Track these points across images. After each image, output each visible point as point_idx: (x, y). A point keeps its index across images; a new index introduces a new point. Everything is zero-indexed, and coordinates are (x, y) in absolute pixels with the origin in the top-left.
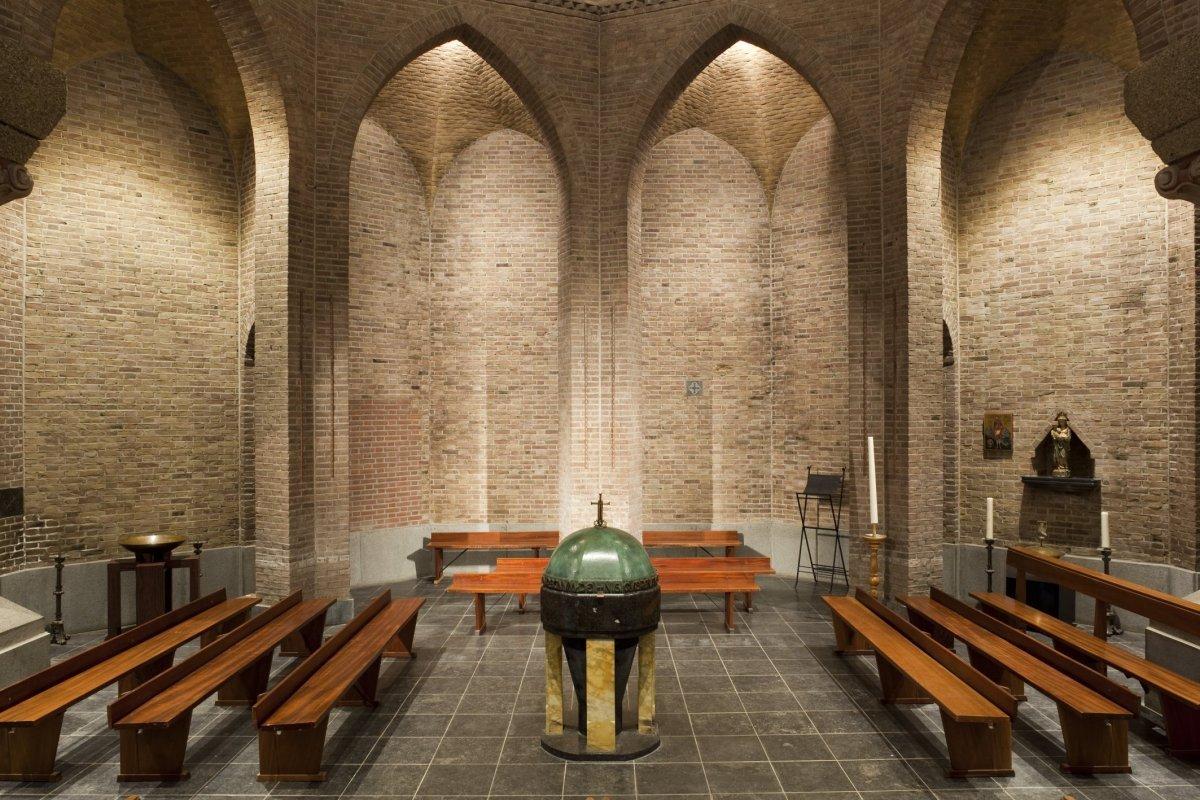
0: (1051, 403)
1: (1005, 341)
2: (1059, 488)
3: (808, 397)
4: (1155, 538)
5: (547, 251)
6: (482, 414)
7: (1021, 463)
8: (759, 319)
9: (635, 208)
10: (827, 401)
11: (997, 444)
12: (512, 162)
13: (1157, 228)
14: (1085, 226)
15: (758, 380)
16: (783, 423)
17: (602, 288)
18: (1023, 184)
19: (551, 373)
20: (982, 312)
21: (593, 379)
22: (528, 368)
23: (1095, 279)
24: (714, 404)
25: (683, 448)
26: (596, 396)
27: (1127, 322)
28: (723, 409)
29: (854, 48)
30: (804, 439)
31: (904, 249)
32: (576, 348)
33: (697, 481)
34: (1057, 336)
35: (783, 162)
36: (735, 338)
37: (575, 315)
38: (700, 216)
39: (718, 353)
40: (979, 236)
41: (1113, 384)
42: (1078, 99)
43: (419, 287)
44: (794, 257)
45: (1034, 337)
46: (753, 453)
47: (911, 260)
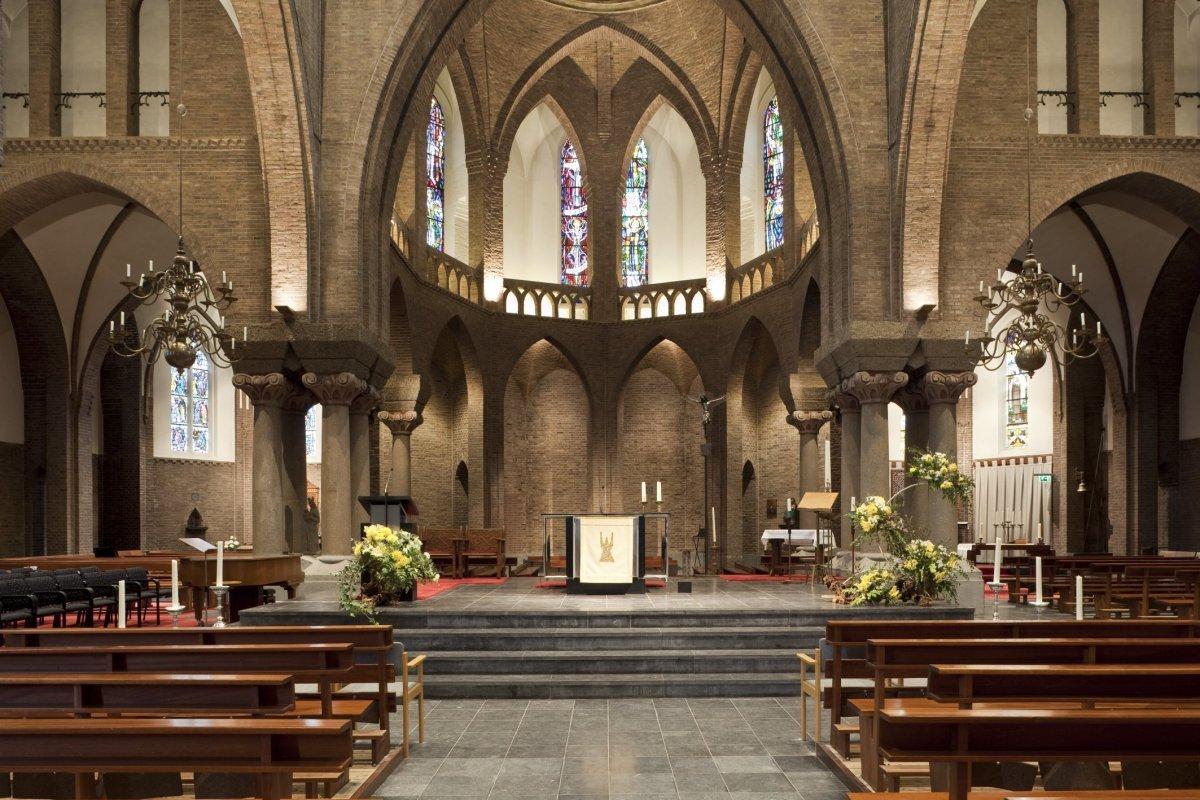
6: (551, 502)
9: (621, 411)
16: (690, 506)
32: (596, 472)
43: (521, 443)
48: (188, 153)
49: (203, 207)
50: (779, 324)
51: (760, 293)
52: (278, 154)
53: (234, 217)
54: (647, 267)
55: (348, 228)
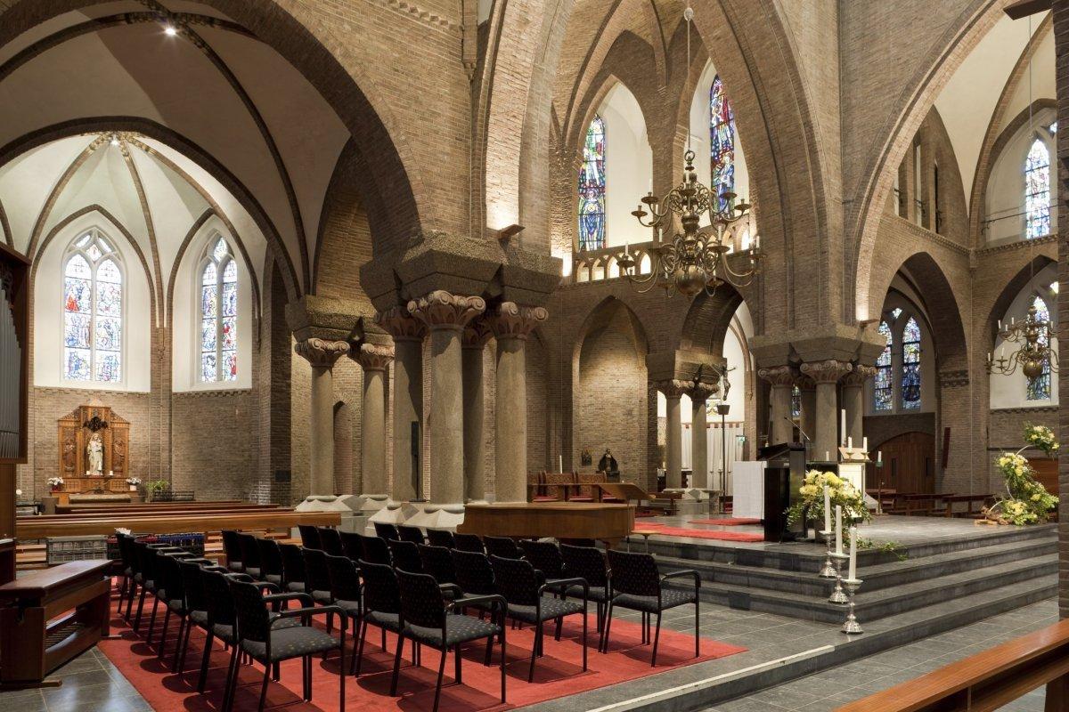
23: (618, 405)
31: (571, 392)
48: (387, 12)
49: (403, 83)
52: (511, 58)
53: (435, 107)
55: (540, 156)
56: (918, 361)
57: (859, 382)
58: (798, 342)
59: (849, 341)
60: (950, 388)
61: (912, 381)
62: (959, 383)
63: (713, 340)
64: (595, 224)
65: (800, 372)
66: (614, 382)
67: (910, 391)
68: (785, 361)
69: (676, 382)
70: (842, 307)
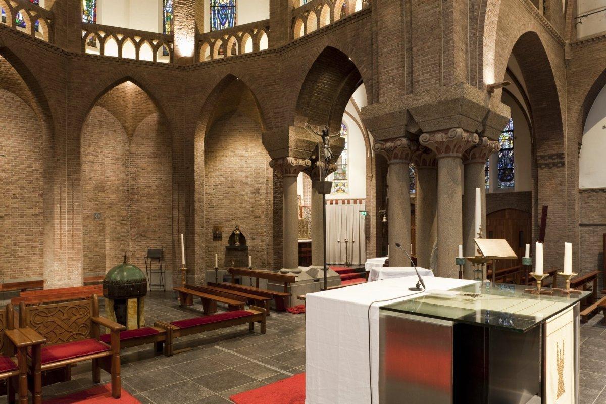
0: (234, 222)
1: (220, 202)
2: (236, 249)
3: (146, 220)
4: (263, 263)
5: (26, 151)
7: (225, 242)
8: (125, 188)
10: (154, 221)
11: (217, 236)
12: (6, 106)
13: (263, 171)
14: (244, 167)
15: (124, 213)
16: (136, 230)
17: (68, 173)
18: (225, 151)
19: (28, 208)
20: (213, 192)
21: (64, 212)
22: (16, 206)
23: (246, 184)
24: (106, 223)
25: (92, 241)
26: (65, 219)
27: (255, 198)
28: (110, 225)
29: (175, 97)
30: (145, 236)
31: (193, 171)
33: (98, 255)
34: (236, 201)
35: (136, 127)
36: (115, 196)
37: (56, 184)
38: (100, 144)
39: (107, 201)
40: (211, 166)
41: (252, 217)
42: (242, 128)
44: (140, 165)
45: (229, 201)
46: (122, 242)
47: (196, 174)
50: (263, 84)
51: (315, 33)
54: (95, 15)
56: (511, 147)
57: (483, 158)
58: (416, 109)
59: (474, 106)
60: (546, 170)
61: (506, 164)
62: (555, 165)
63: (330, 119)
64: (226, 15)
65: (419, 144)
66: (243, 162)
67: (504, 173)
68: (402, 132)
69: (291, 159)
70: (467, 67)
